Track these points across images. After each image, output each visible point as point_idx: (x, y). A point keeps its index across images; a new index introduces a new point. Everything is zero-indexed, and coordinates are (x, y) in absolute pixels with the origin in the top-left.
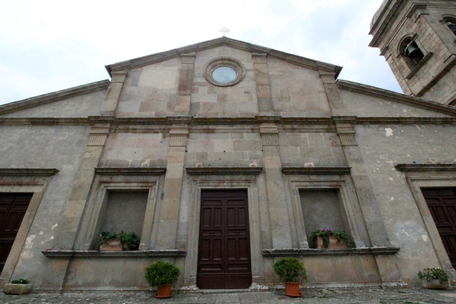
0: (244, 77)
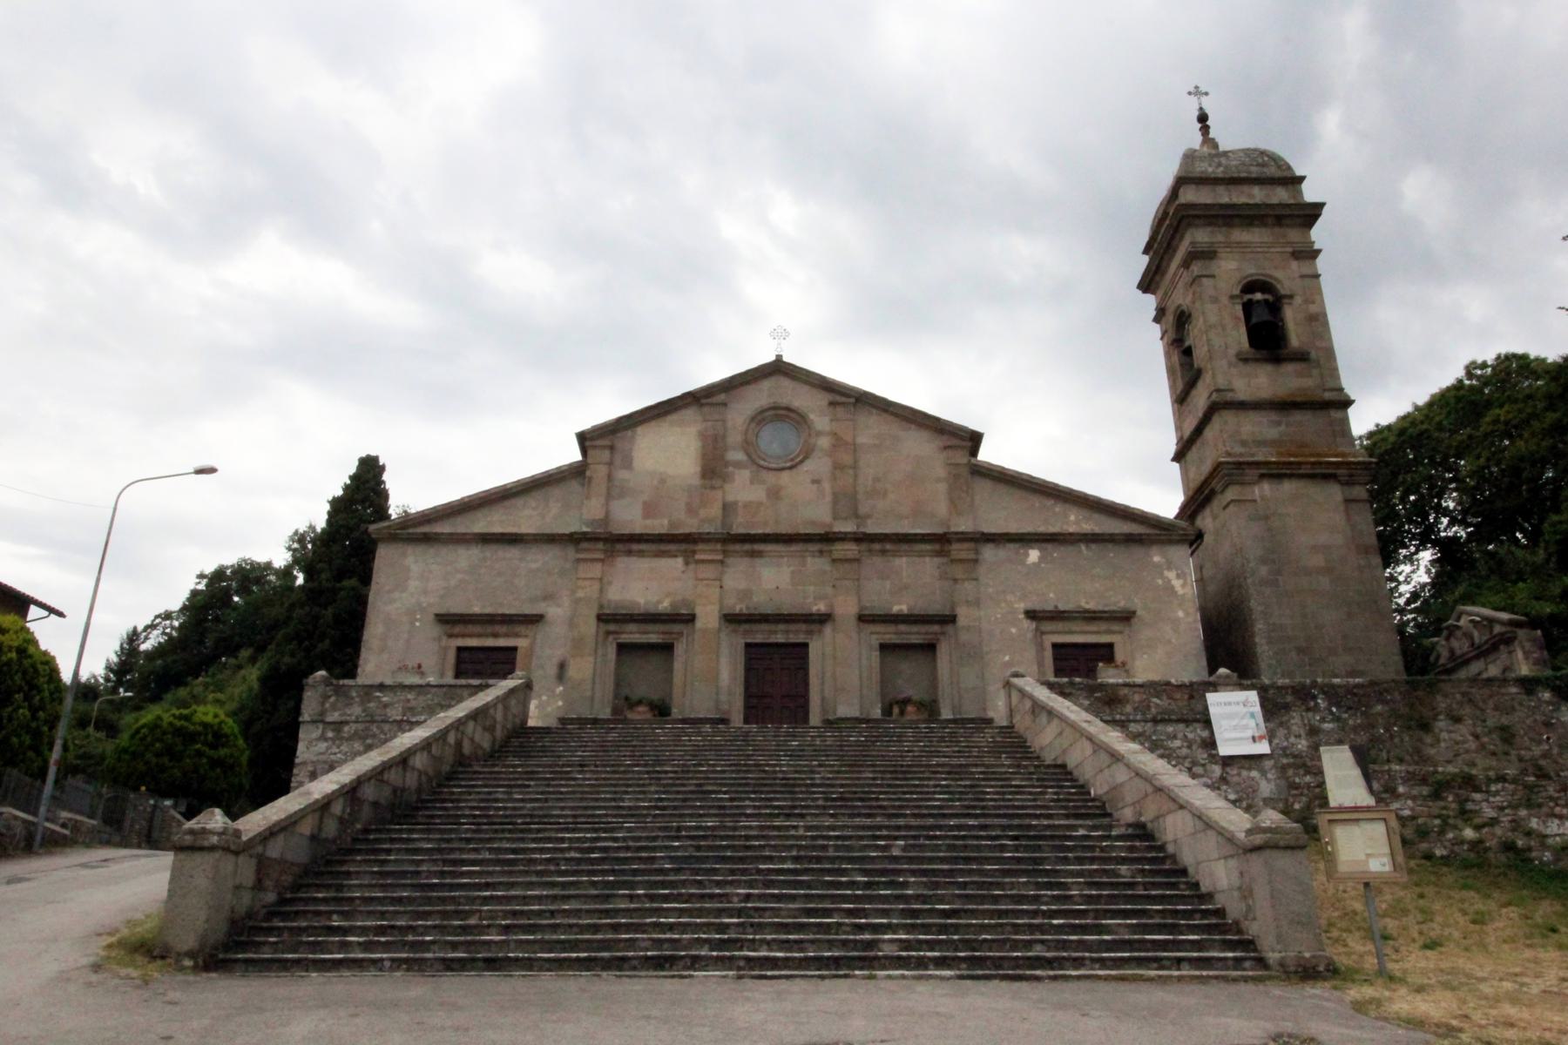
0: (813, 450)
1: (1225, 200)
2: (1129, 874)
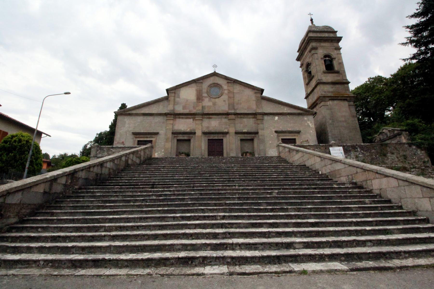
1: (319, 36)
2: (369, 202)
